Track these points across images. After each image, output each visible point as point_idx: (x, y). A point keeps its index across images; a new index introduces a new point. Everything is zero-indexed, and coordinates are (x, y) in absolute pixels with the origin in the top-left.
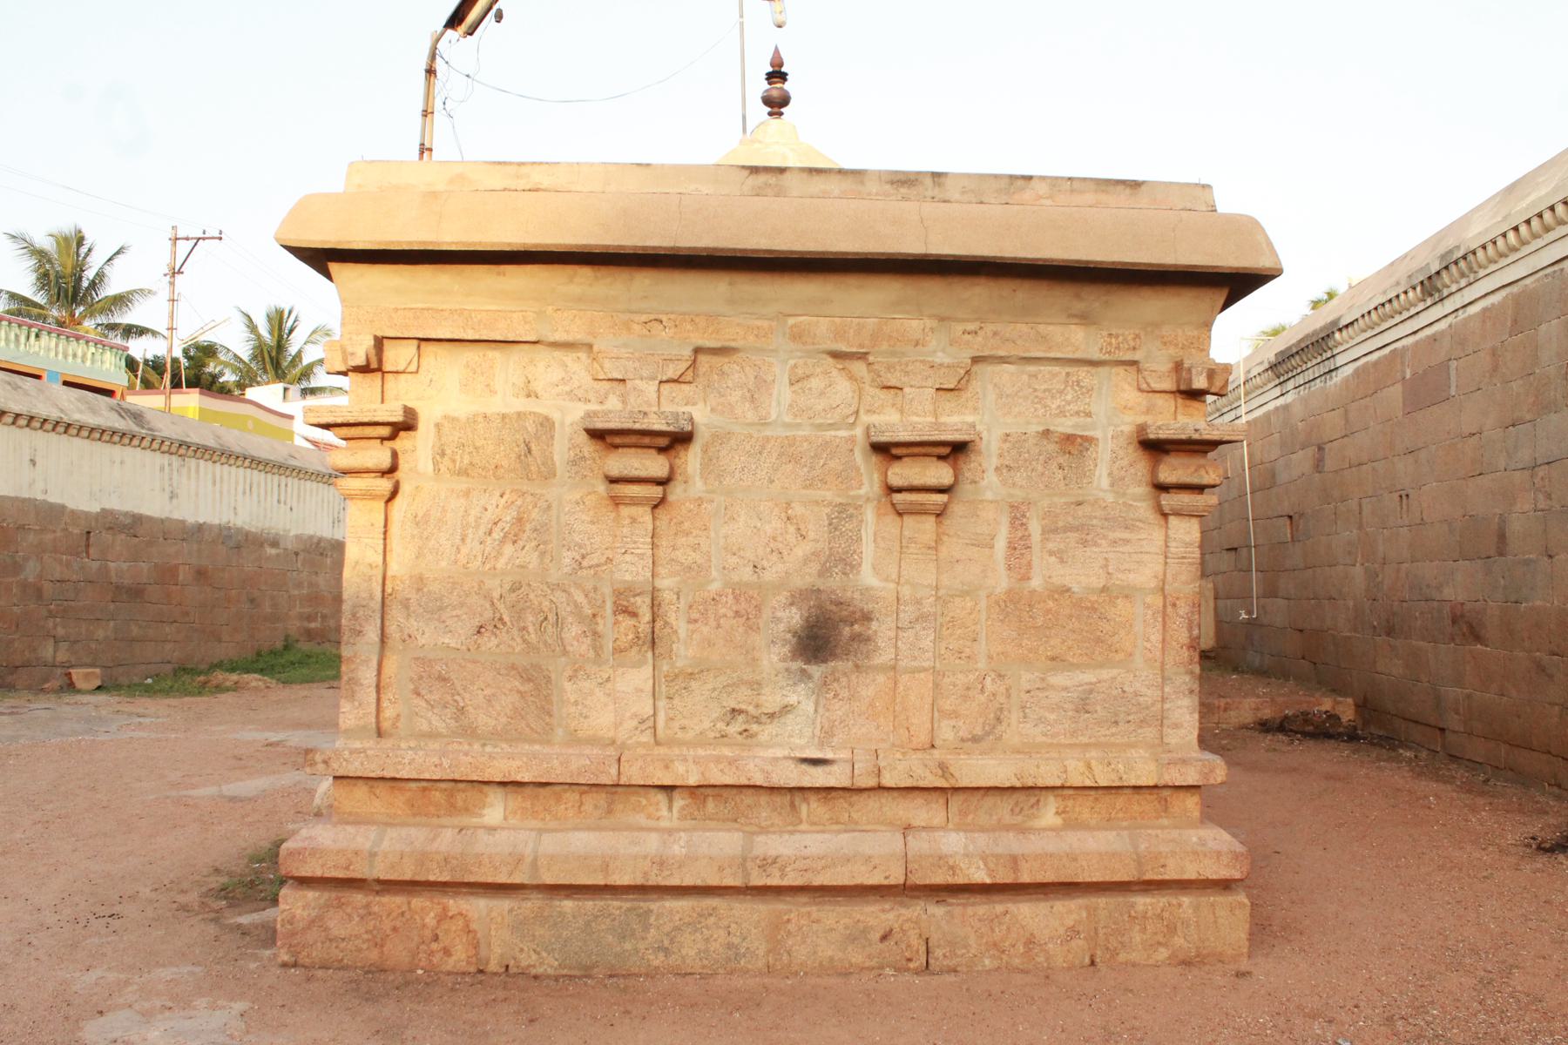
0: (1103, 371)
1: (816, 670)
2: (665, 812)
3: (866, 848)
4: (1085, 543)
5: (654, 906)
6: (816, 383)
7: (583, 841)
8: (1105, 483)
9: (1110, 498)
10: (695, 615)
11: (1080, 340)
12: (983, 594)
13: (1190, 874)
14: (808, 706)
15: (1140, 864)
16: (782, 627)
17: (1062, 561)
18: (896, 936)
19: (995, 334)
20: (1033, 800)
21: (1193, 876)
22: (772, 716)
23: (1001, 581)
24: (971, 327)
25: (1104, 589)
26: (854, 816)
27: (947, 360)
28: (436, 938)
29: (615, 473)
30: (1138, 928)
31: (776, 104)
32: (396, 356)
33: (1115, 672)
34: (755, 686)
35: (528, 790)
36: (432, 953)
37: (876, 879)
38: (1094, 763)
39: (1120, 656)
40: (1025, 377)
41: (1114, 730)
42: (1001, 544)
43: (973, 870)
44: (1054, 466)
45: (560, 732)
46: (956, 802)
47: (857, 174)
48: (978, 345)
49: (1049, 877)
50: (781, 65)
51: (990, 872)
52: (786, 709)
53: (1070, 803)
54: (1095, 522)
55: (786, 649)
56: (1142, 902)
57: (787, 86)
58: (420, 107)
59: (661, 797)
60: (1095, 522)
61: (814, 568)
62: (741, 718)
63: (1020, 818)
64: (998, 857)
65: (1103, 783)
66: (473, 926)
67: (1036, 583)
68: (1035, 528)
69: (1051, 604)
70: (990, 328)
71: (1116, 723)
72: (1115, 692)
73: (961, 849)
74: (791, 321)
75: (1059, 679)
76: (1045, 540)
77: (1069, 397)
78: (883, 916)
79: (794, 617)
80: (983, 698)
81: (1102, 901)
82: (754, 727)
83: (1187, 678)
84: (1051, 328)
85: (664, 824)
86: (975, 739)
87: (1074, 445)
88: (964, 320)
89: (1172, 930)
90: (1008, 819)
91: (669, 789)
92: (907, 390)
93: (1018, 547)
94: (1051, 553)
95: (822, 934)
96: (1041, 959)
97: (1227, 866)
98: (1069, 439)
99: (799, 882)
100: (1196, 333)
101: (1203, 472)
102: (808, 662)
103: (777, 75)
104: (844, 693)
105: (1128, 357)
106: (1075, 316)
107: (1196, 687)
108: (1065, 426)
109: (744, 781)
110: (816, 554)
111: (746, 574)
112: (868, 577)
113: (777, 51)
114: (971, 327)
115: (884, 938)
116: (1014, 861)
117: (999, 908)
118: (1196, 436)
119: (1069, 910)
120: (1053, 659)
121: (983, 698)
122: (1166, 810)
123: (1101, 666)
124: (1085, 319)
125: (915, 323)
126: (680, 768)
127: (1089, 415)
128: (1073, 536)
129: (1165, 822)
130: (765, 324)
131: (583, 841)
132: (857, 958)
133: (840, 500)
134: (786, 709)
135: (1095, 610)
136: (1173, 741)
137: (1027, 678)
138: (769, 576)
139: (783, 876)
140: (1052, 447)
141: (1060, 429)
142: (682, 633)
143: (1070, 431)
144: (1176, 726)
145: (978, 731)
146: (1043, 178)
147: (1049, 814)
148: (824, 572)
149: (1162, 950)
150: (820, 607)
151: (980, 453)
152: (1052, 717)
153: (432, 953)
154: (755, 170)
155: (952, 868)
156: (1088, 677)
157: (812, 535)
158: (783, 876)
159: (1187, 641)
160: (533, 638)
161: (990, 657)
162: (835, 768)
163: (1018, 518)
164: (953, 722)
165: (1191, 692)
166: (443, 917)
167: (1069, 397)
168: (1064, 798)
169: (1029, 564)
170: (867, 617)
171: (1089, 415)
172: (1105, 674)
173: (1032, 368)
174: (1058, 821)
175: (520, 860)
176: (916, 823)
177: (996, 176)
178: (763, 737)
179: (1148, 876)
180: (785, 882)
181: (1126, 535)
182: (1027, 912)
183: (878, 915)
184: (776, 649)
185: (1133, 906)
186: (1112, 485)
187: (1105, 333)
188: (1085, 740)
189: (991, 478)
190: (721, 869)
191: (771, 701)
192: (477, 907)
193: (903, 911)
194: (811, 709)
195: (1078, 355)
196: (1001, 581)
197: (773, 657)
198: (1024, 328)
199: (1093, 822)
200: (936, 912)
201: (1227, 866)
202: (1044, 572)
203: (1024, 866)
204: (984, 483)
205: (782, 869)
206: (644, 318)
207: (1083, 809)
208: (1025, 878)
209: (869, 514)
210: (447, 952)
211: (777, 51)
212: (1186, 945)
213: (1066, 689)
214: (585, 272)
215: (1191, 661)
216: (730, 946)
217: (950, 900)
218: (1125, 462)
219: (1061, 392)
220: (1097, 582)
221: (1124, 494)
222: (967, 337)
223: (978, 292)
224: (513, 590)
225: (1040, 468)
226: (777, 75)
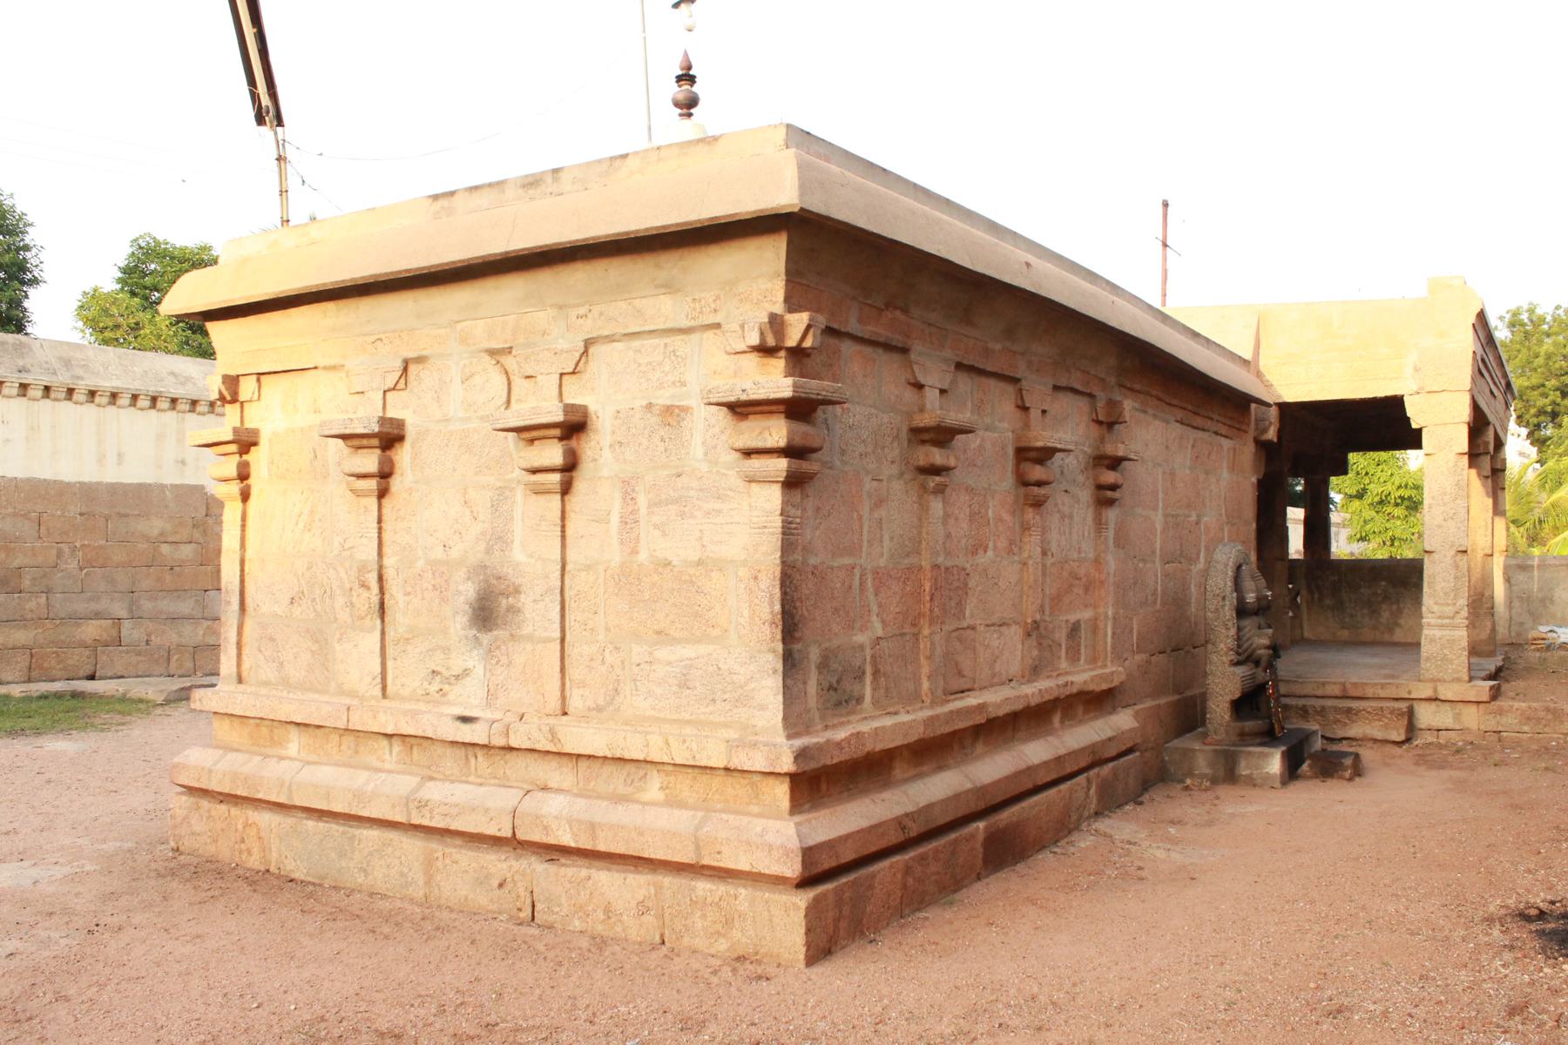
0: (695, 337)
1: (486, 638)
2: (387, 756)
3: (478, 800)
4: (682, 515)
5: (357, 832)
6: (477, 380)
7: (325, 774)
8: (699, 452)
9: (705, 468)
10: (409, 589)
11: (666, 309)
12: (601, 568)
13: (743, 865)
14: (479, 670)
15: (698, 848)
16: (462, 599)
17: (664, 534)
18: (509, 886)
19: (601, 314)
20: (641, 773)
21: (747, 868)
22: (457, 677)
23: (614, 555)
24: (582, 311)
25: (700, 563)
26: (508, 772)
27: (566, 346)
28: (243, 841)
29: (537, 464)
30: (699, 914)
31: (688, 105)
32: (247, 389)
33: (711, 647)
34: (446, 650)
35: (310, 730)
36: (241, 852)
37: (491, 831)
38: (671, 740)
39: (716, 632)
40: (631, 353)
41: (711, 708)
42: (615, 519)
43: (560, 833)
44: (656, 439)
45: (333, 684)
46: (583, 764)
47: (499, 185)
48: (589, 328)
49: (620, 849)
50: (690, 68)
51: (575, 835)
52: (466, 672)
53: (672, 778)
54: (692, 493)
55: (465, 619)
56: (703, 887)
57: (695, 89)
58: (277, 189)
59: (385, 742)
60: (692, 493)
61: (482, 546)
62: (438, 678)
63: (630, 789)
64: (579, 822)
65: (678, 761)
66: (263, 834)
67: (643, 556)
68: (642, 501)
69: (656, 578)
70: (596, 309)
71: (714, 700)
72: (711, 669)
73: (559, 813)
74: (459, 327)
75: (662, 653)
76: (650, 513)
77: (667, 368)
78: (499, 865)
79: (468, 591)
80: (604, 669)
81: (667, 880)
82: (446, 687)
83: (770, 657)
84: (644, 301)
85: (387, 766)
86: (599, 709)
87: (672, 414)
88: (578, 305)
89: (728, 922)
90: (621, 790)
91: (389, 736)
92: (540, 378)
93: (629, 522)
94: (656, 526)
95: (463, 876)
96: (619, 928)
97: (778, 861)
98: (668, 410)
99: (441, 825)
100: (769, 285)
101: (766, 434)
102: (479, 631)
103: (687, 78)
104: (504, 660)
105: (711, 319)
106: (662, 286)
107: (780, 666)
108: (664, 398)
109: (420, 733)
110: (483, 533)
111: (438, 553)
112: (518, 554)
113: (686, 54)
114: (582, 311)
115: (501, 885)
116: (593, 827)
117: (584, 872)
118: (744, 397)
119: (637, 885)
120: (659, 633)
121: (604, 669)
122: (757, 796)
123: (699, 641)
124: (669, 287)
125: (541, 314)
126: (382, 717)
127: (683, 384)
128: (673, 509)
129: (755, 809)
130: (443, 331)
131: (325, 774)
132: (483, 900)
133: (498, 484)
134: (466, 672)
135: (692, 582)
136: (760, 724)
137: (638, 651)
138: (455, 553)
139: (431, 818)
140: (654, 420)
141: (660, 402)
142: (401, 604)
143: (669, 403)
144: (763, 708)
145: (601, 702)
146: (636, 153)
147: (653, 788)
148: (488, 551)
149: (722, 940)
150: (486, 581)
151: (596, 431)
152: (659, 691)
153: (241, 852)
154: (435, 197)
155: (546, 828)
156: (688, 652)
157: (481, 517)
158: (431, 818)
159: (769, 617)
160: (319, 607)
161: (607, 629)
162: (476, 726)
163: (629, 497)
164: (581, 691)
165: (775, 672)
166: (246, 825)
167: (667, 368)
168: (667, 774)
169: (638, 539)
170: (517, 591)
171: (683, 384)
172: (703, 649)
173: (636, 344)
174: (660, 796)
175: (282, 785)
176: (552, 784)
177: (599, 161)
178: (451, 697)
179: (706, 862)
180: (433, 824)
181: (718, 505)
182: (606, 880)
183: (498, 864)
184: (458, 618)
185: (693, 889)
186: (706, 454)
187: (689, 299)
188: (687, 716)
189: (607, 453)
190: (394, 806)
191: (457, 665)
192: (265, 818)
193: (514, 863)
194: (481, 672)
195: (669, 325)
196: (615, 556)
197: (459, 624)
198: (623, 305)
199: (691, 801)
200: (538, 867)
201: (778, 861)
202: (653, 545)
203: (601, 835)
204: (602, 461)
205: (431, 811)
206: (373, 338)
207: (684, 786)
208: (602, 848)
209: (519, 495)
210: (249, 853)
211: (686, 54)
212: (744, 940)
213: (669, 663)
214: (330, 307)
215: (773, 639)
216: (402, 875)
217: (563, 861)
218: (717, 430)
219: (660, 364)
220: (694, 556)
221: (716, 463)
222: (581, 321)
223: (578, 275)
224: (309, 569)
225: (645, 442)
226: (687, 78)
